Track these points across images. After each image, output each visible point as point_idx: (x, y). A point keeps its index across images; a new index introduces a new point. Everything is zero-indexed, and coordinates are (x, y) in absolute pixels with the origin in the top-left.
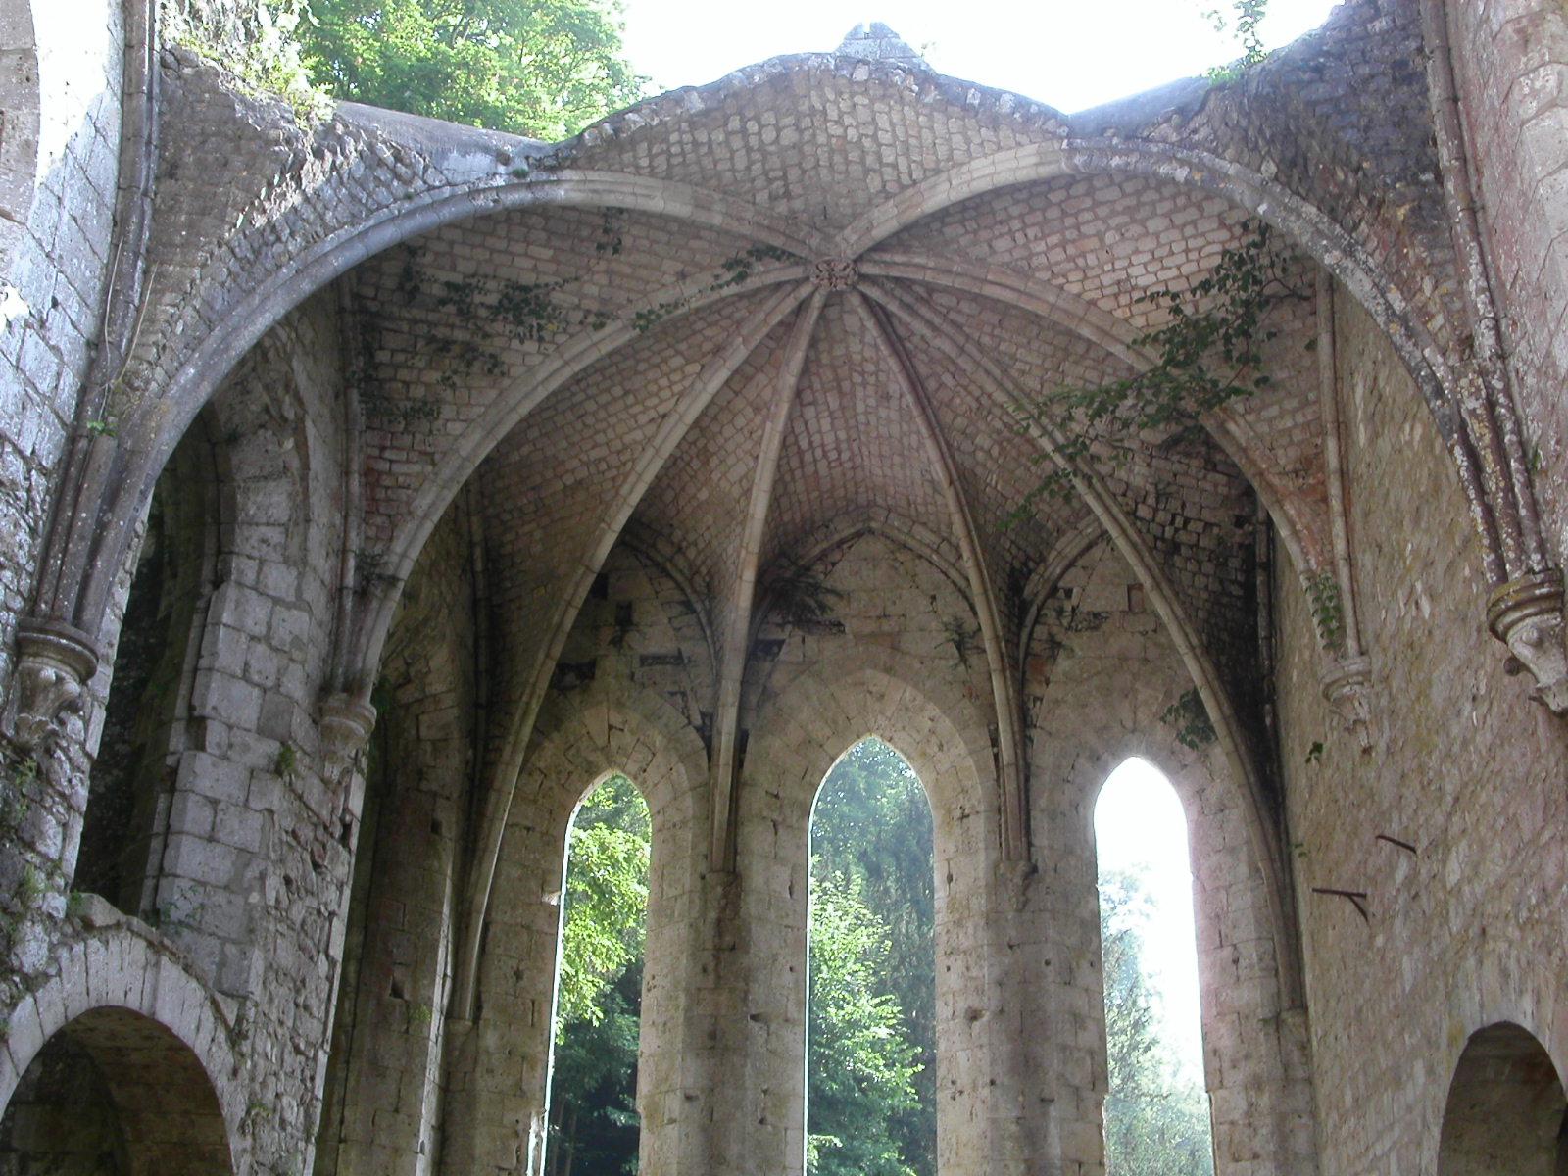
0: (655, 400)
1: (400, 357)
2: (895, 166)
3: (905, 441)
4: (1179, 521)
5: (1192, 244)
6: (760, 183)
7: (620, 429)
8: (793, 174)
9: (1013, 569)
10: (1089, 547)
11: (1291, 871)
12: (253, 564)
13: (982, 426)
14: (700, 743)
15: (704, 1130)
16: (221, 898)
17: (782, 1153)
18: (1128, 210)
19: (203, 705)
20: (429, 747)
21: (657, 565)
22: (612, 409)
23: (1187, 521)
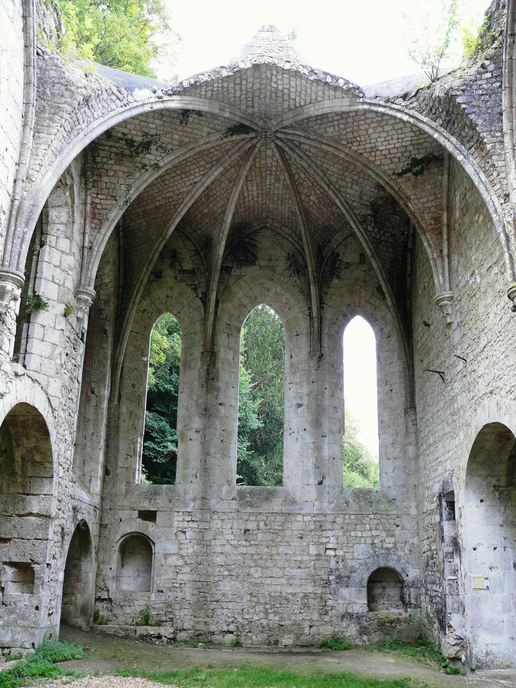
0: (193, 177)
1: (105, 160)
2: (295, 100)
3: (284, 196)
4: (382, 232)
5: (400, 136)
6: (244, 102)
7: (179, 186)
8: (256, 99)
9: (319, 245)
10: (346, 238)
11: (413, 360)
12: (54, 238)
14: (201, 304)
15: (202, 443)
16: (47, 361)
17: (229, 452)
18: (378, 122)
19: (39, 291)
20: (103, 302)
21: (186, 235)
22: (176, 179)
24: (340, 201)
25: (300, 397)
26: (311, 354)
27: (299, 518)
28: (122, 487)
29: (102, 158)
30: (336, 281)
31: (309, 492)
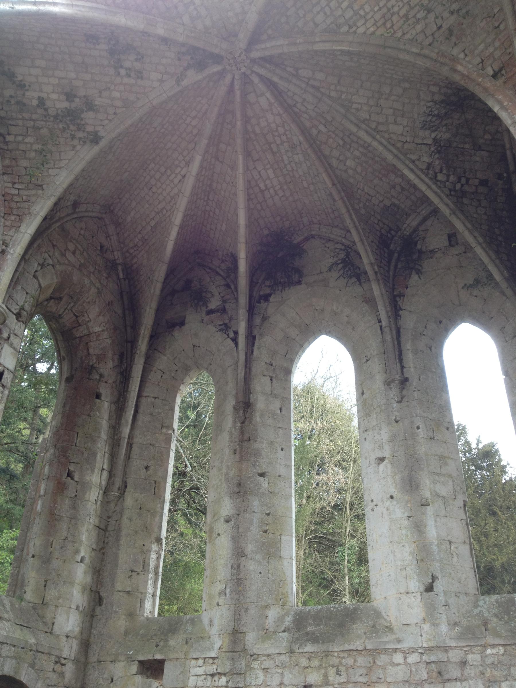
1: (20, 138)
4: (463, 180)
9: (382, 234)
13: (348, 154)
14: (234, 346)
17: (279, 550)
23: (468, 180)
24: (381, 143)
25: (381, 448)
26: (388, 383)
27: (398, 658)
28: (121, 623)
29: (16, 135)
30: (415, 277)
31: (409, 606)
